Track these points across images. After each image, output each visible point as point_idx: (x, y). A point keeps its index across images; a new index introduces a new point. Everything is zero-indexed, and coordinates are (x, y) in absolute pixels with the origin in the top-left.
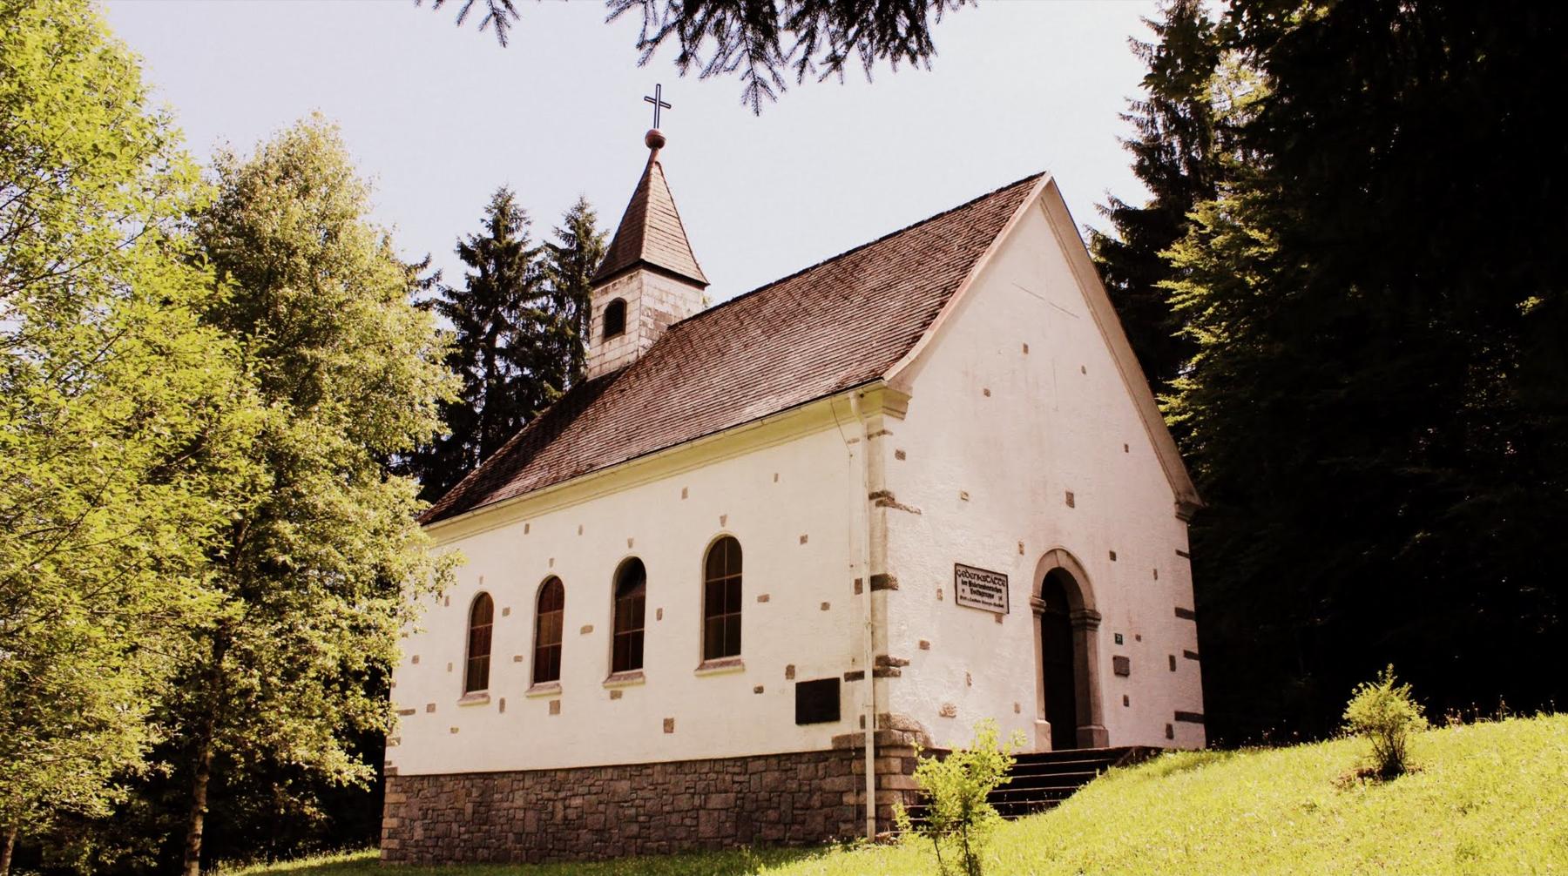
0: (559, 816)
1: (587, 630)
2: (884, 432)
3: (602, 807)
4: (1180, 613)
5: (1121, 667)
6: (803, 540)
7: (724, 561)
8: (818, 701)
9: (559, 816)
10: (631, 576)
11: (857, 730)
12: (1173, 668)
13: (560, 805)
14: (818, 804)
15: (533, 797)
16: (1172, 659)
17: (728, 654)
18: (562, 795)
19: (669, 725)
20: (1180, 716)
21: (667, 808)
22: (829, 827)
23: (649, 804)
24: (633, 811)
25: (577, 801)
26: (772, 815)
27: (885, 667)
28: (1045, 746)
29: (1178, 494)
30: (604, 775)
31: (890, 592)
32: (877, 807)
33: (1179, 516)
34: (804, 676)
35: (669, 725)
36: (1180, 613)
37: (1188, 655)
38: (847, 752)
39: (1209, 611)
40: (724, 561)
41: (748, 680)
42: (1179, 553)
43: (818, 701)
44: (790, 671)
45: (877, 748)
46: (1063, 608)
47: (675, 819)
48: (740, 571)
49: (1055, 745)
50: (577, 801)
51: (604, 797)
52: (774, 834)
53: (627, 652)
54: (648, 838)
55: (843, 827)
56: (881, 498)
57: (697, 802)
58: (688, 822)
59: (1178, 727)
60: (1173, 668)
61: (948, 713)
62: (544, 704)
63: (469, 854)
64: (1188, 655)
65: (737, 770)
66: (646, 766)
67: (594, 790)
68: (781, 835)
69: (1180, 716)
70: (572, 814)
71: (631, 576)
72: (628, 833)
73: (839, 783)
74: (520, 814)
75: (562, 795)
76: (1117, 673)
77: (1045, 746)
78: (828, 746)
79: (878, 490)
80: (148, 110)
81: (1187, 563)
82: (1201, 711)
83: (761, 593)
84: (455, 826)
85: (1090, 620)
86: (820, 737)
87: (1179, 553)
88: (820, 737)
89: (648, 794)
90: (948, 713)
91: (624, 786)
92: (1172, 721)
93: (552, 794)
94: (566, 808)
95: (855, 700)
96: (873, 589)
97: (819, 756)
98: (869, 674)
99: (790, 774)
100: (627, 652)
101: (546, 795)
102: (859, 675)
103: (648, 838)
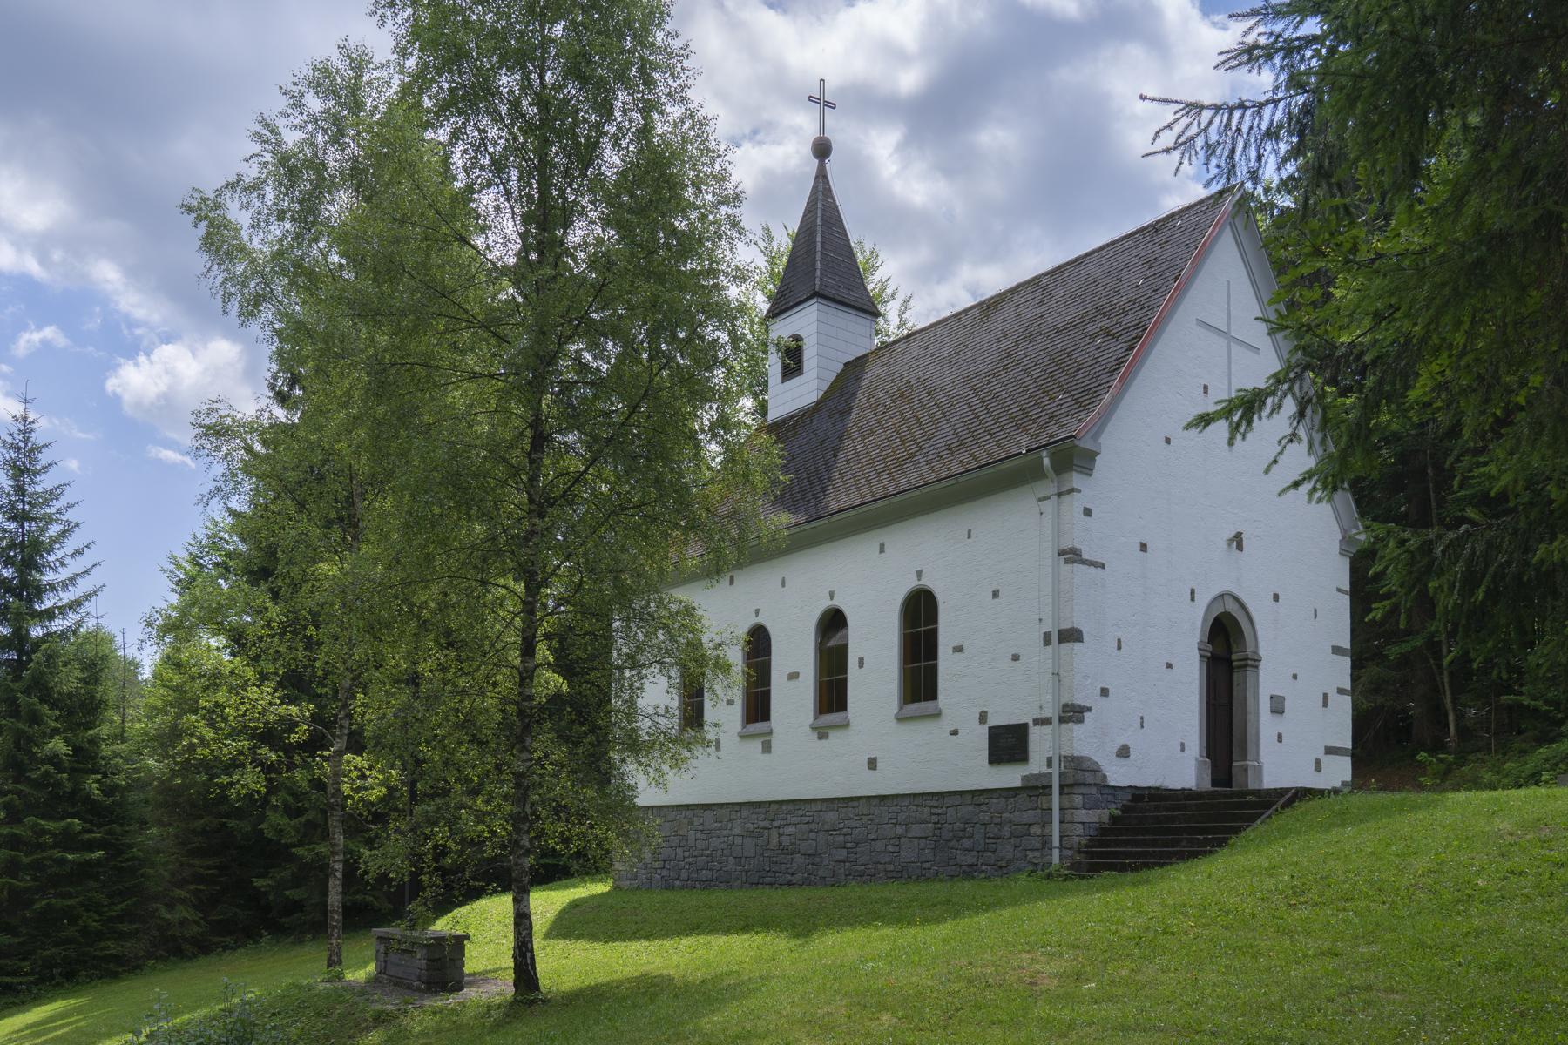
0: (774, 842)
1: (794, 676)
2: (1072, 490)
3: (813, 835)
4: (1337, 650)
5: (1278, 707)
6: (995, 594)
7: (920, 612)
8: (1008, 743)
9: (774, 842)
10: (833, 622)
11: (1045, 770)
12: (1325, 704)
13: (774, 833)
14: (1008, 835)
15: (750, 826)
16: (1325, 696)
17: (926, 699)
18: (776, 824)
19: (872, 764)
20: (1330, 751)
21: (872, 837)
22: (1019, 855)
23: (855, 832)
24: (841, 838)
25: (790, 830)
26: (967, 843)
27: (1073, 713)
28: (1207, 785)
29: (1344, 532)
30: (814, 807)
31: (1077, 645)
32: (1061, 837)
33: (1343, 552)
34: (994, 721)
35: (872, 764)
36: (1337, 650)
37: (1341, 691)
38: (1035, 789)
39: (1367, 647)
40: (920, 612)
41: (946, 724)
42: (1339, 590)
43: (1008, 743)
44: (983, 717)
45: (1062, 787)
46: (1226, 646)
47: (879, 845)
48: (936, 622)
49: (1214, 783)
50: (790, 830)
51: (813, 826)
52: (970, 859)
53: (832, 695)
54: (855, 862)
55: (1030, 854)
56: (1072, 556)
57: (899, 830)
58: (890, 848)
59: (1327, 761)
60: (1325, 704)
61: (1124, 752)
62: (757, 745)
63: (694, 875)
64: (1341, 691)
65: (934, 803)
66: (852, 799)
67: (806, 819)
68: (974, 861)
69: (1330, 751)
70: (786, 840)
71: (833, 622)
72: (838, 858)
73: (1027, 816)
74: (739, 841)
75: (776, 824)
76: (1273, 712)
77: (1207, 785)
78: (1018, 783)
79: (1066, 545)
80: (174, 599)
81: (1346, 600)
82: (1349, 745)
83: (956, 644)
84: (679, 851)
85: (1251, 663)
86: (1010, 776)
87: (1339, 590)
88: (1010, 776)
89: (854, 824)
90: (1124, 752)
91: (831, 816)
92: (1320, 754)
93: (766, 824)
94: (780, 835)
95: (1041, 744)
96: (1061, 641)
97: (1013, 792)
98: (1056, 720)
99: (984, 808)
100: (832, 695)
101: (762, 824)
102: (1044, 722)
103: (855, 862)
